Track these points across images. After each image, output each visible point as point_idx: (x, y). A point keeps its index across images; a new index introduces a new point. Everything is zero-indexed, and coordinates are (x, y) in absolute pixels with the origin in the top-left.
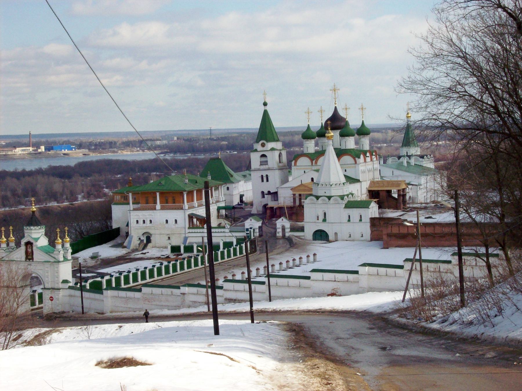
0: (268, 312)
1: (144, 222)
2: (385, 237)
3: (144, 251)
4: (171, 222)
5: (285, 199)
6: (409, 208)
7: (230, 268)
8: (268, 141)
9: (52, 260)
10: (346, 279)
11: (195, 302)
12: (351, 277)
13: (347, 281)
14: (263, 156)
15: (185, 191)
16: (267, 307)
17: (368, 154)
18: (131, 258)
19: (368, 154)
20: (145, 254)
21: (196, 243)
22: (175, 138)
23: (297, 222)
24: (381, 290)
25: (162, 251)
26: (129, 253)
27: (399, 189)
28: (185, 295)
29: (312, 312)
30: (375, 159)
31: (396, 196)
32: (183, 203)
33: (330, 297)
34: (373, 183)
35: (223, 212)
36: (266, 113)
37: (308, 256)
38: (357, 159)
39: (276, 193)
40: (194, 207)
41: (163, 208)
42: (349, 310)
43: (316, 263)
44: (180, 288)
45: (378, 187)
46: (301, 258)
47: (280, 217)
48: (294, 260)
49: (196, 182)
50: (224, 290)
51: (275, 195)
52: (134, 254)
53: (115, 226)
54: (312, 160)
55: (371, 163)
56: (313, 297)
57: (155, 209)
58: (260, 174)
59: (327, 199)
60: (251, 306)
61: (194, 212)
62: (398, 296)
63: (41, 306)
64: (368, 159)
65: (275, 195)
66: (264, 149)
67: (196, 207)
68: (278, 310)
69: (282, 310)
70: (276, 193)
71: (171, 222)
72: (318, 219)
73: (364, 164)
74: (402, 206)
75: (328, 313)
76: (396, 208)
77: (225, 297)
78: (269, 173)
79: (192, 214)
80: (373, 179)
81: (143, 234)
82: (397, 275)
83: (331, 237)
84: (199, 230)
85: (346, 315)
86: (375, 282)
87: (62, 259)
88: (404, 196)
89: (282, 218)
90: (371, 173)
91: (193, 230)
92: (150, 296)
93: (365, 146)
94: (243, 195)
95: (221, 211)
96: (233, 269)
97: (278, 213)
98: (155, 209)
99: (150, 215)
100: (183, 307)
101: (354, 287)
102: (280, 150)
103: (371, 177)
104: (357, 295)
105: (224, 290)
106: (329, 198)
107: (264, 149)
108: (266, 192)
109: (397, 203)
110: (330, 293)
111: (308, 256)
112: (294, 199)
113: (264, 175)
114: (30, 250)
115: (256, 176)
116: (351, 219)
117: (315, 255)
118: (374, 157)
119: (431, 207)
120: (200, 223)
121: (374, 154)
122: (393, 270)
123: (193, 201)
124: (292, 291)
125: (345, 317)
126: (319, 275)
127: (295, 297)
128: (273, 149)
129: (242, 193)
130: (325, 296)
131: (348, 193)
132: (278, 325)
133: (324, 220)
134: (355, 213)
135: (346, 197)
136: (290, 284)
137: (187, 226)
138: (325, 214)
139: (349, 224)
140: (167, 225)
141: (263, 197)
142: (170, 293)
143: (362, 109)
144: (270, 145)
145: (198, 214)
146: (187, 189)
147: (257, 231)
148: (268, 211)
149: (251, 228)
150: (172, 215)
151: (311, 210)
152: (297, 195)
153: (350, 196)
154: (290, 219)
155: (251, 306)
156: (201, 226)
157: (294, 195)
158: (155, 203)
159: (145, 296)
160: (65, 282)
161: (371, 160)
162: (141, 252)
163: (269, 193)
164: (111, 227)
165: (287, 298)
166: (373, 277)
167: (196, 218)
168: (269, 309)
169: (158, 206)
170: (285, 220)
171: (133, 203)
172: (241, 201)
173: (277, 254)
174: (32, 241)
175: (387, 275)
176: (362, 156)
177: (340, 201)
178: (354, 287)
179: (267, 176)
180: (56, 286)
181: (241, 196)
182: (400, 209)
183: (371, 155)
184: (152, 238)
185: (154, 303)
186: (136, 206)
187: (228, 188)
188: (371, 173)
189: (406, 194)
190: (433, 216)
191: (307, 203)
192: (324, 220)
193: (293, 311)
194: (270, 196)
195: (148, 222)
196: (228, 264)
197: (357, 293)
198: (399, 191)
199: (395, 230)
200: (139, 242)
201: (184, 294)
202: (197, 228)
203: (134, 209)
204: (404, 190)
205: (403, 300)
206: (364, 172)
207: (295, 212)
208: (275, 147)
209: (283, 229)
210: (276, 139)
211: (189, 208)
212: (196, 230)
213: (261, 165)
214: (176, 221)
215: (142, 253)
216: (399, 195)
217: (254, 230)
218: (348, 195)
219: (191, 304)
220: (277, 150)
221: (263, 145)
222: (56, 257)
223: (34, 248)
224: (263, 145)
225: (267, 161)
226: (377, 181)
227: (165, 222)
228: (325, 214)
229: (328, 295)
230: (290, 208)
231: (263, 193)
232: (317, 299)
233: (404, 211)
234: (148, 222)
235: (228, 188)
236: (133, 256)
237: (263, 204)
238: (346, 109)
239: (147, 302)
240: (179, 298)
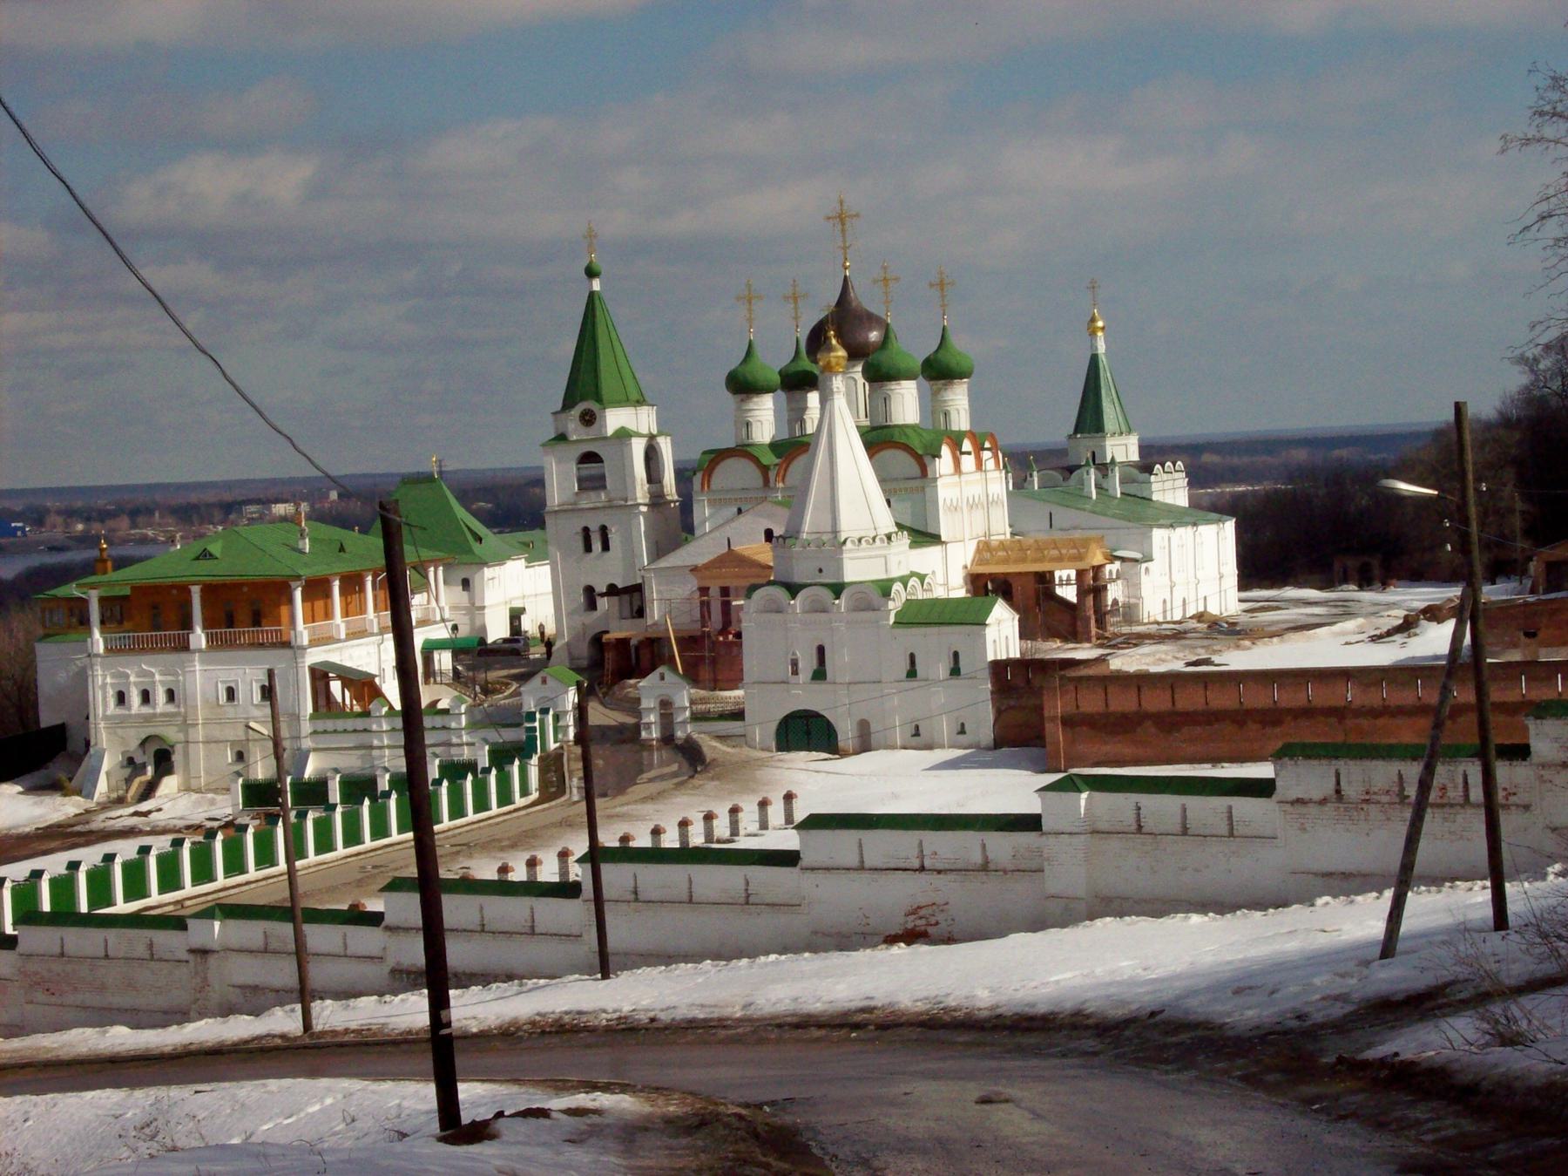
0: (592, 1030)
1: (146, 697)
2: (1056, 733)
3: (145, 806)
5: (668, 606)
6: (1116, 636)
7: (458, 853)
10: (977, 858)
11: (255, 989)
12: (1002, 845)
13: (985, 867)
14: (590, 458)
15: (298, 577)
16: (585, 1007)
17: (967, 445)
18: (91, 832)
19: (967, 445)
20: (146, 814)
21: (336, 771)
22: (334, 495)
23: (714, 689)
24: (1158, 907)
25: (212, 802)
26: (87, 812)
27: (1082, 565)
28: (212, 960)
29: (820, 1026)
30: (990, 464)
31: (1069, 593)
33: (900, 949)
34: (984, 548)
37: (763, 804)
38: (927, 460)
39: (637, 590)
41: (216, 643)
42: (1042, 1009)
43: (819, 686)
44: (184, 928)
45: (1006, 561)
46: (734, 811)
47: (653, 669)
48: (709, 817)
49: (342, 549)
50: (388, 928)
51: (632, 596)
52: (102, 816)
53: (47, 719)
55: (978, 476)
56: (814, 949)
57: (184, 647)
58: (578, 524)
59: (827, 594)
60: (439, 1004)
62: (1359, 920)
64: (968, 462)
67: (339, 641)
68: (644, 1018)
69: (665, 1017)
70: (637, 590)
72: (795, 672)
73: (956, 477)
74: (1094, 630)
75: (915, 1033)
76: (1074, 634)
77: (391, 962)
79: (326, 663)
80: (988, 534)
81: (143, 743)
82: (1239, 829)
83: (846, 732)
84: (350, 724)
85: (1031, 1039)
86: (1127, 867)
88: (1098, 591)
89: (661, 669)
90: (979, 516)
92: (57, 967)
93: (954, 416)
94: (523, 610)
95: (436, 656)
96: (470, 856)
97: (645, 656)
100: (202, 1015)
101: (1019, 893)
102: (652, 437)
103: (979, 530)
104: (1040, 935)
105: (388, 928)
108: (601, 588)
109: (1074, 618)
110: (898, 930)
111: (763, 804)
112: (705, 606)
113: (594, 527)
115: (563, 530)
116: (919, 667)
117: (789, 797)
118: (986, 455)
119: (1194, 630)
120: (357, 697)
121: (987, 445)
122: (1219, 803)
124: (707, 926)
125: (1037, 1052)
126: (842, 845)
127: (725, 953)
129: (517, 604)
130: (874, 946)
131: (906, 572)
132: (630, 1133)
133: (820, 674)
134: (933, 646)
135: (897, 586)
136: (700, 893)
138: (821, 651)
139: (955, 682)
140: (230, 711)
141: (591, 605)
142: (141, 950)
145: (348, 664)
146: (306, 572)
148: (609, 656)
151: (769, 637)
152: (715, 592)
153: (913, 581)
154: (692, 676)
155: (439, 1004)
156: (357, 708)
157: (704, 591)
158: (187, 625)
159: (32, 967)
161: (979, 464)
162: (131, 810)
163: (612, 590)
164: (37, 721)
165: (688, 957)
166: (1114, 844)
167: (339, 677)
168: (595, 1013)
169: (199, 638)
170: (670, 676)
172: (516, 629)
173: (644, 800)
175: (1185, 831)
176: (945, 451)
178: (1019, 893)
181: (516, 616)
182: (1089, 640)
183: (979, 448)
185: (70, 999)
188: (979, 516)
189: (1105, 588)
190: (1216, 659)
191: (750, 613)
192: (820, 674)
193: (721, 1023)
194: (616, 599)
196: (453, 841)
197: (1037, 924)
198: (1080, 574)
199: (1091, 703)
200: (128, 771)
201: (203, 952)
204: (1098, 569)
205: (1388, 946)
207: (711, 653)
209: (666, 705)
210: (634, 396)
211: (316, 642)
212: (340, 724)
215: (136, 814)
216: (1081, 593)
217: (557, 718)
218: (904, 581)
219: (235, 997)
224: (588, 419)
225: (602, 478)
226: (1001, 542)
228: (821, 651)
229: (891, 940)
230: (689, 642)
231: (589, 590)
232: (836, 959)
233: (1101, 646)
235: (466, 584)
236: (98, 823)
237: (591, 633)
238: (795, 299)
239: (40, 996)
240: (183, 972)
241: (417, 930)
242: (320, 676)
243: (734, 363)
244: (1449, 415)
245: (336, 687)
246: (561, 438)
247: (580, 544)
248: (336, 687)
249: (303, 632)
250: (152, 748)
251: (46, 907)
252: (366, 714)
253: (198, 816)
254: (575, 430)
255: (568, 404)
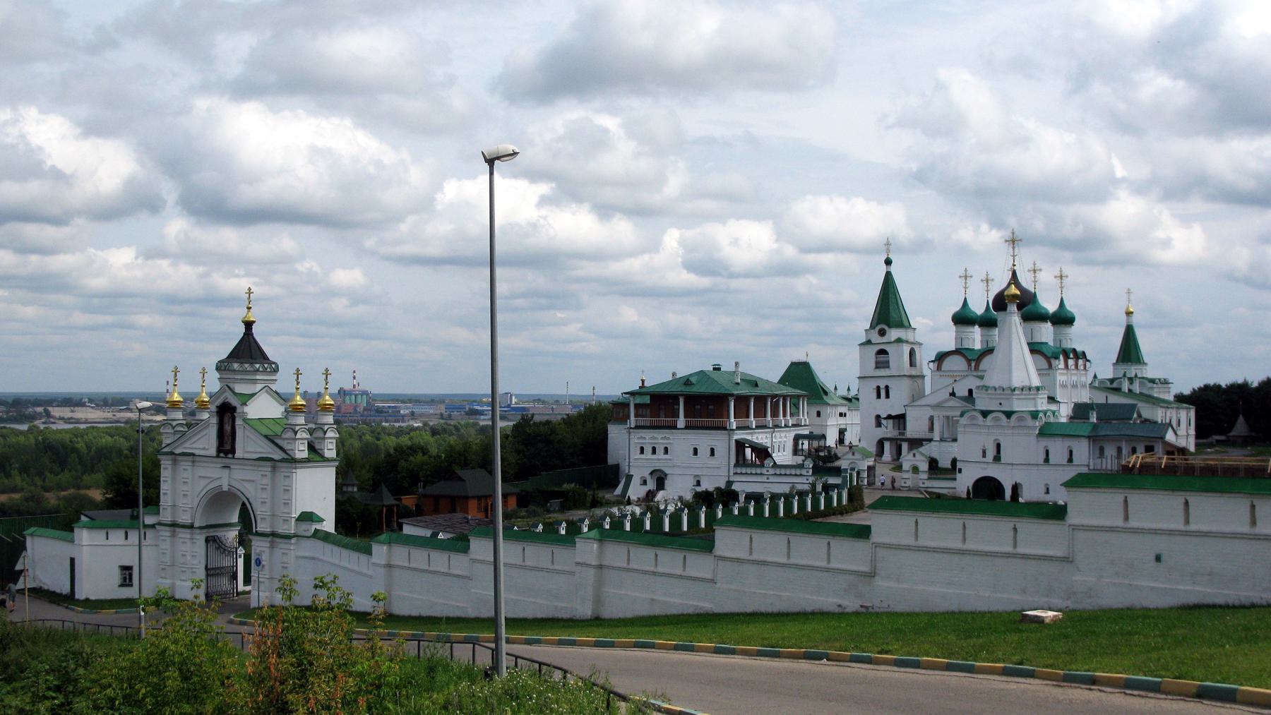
4: (704, 452)
8: (890, 327)
9: (278, 455)
14: (882, 352)
32: (728, 417)
35: (806, 445)
36: (888, 276)
38: (1053, 361)
40: (748, 428)
41: (688, 427)
43: (996, 466)
54: (969, 361)
57: (675, 427)
58: (873, 384)
59: (1003, 417)
61: (749, 437)
63: (248, 588)
64: (1071, 362)
65: (900, 419)
66: (884, 339)
71: (704, 452)
72: (984, 456)
78: (893, 384)
81: (651, 473)
87: (301, 451)
91: (744, 471)
98: (675, 427)
99: (665, 438)
106: (1009, 414)
107: (884, 339)
113: (882, 386)
114: (228, 428)
123: (748, 416)
128: (899, 341)
133: (997, 458)
135: (1041, 415)
137: (733, 461)
138: (998, 446)
139: (1046, 468)
143: (1061, 277)
144: (894, 334)
147: (865, 475)
149: (853, 469)
150: (704, 440)
160: (307, 517)
163: (889, 417)
169: (681, 422)
171: (636, 416)
174: (234, 401)
176: (1061, 357)
177: (1030, 422)
179: (887, 387)
180: (281, 529)
184: (667, 482)
186: (642, 421)
187: (819, 414)
192: (997, 458)
194: (891, 421)
195: (660, 450)
202: (753, 465)
203: (637, 427)
206: (1064, 386)
208: (904, 338)
210: (906, 324)
213: (877, 367)
214: (712, 450)
217: (858, 473)
220: (907, 342)
221: (882, 333)
222: (287, 447)
223: (238, 422)
224: (882, 333)
227: (692, 451)
231: (878, 417)
234: (660, 450)
235: (819, 414)
241: (258, 534)
242: (740, 445)
243: (957, 307)
244: (966, 394)
245: (748, 451)
246: (869, 342)
247: (875, 394)
248: (748, 451)
249: (733, 423)
250: (656, 475)
251: (667, 529)
252: (762, 466)
253: (785, 489)
254: (875, 337)
255: (872, 327)
